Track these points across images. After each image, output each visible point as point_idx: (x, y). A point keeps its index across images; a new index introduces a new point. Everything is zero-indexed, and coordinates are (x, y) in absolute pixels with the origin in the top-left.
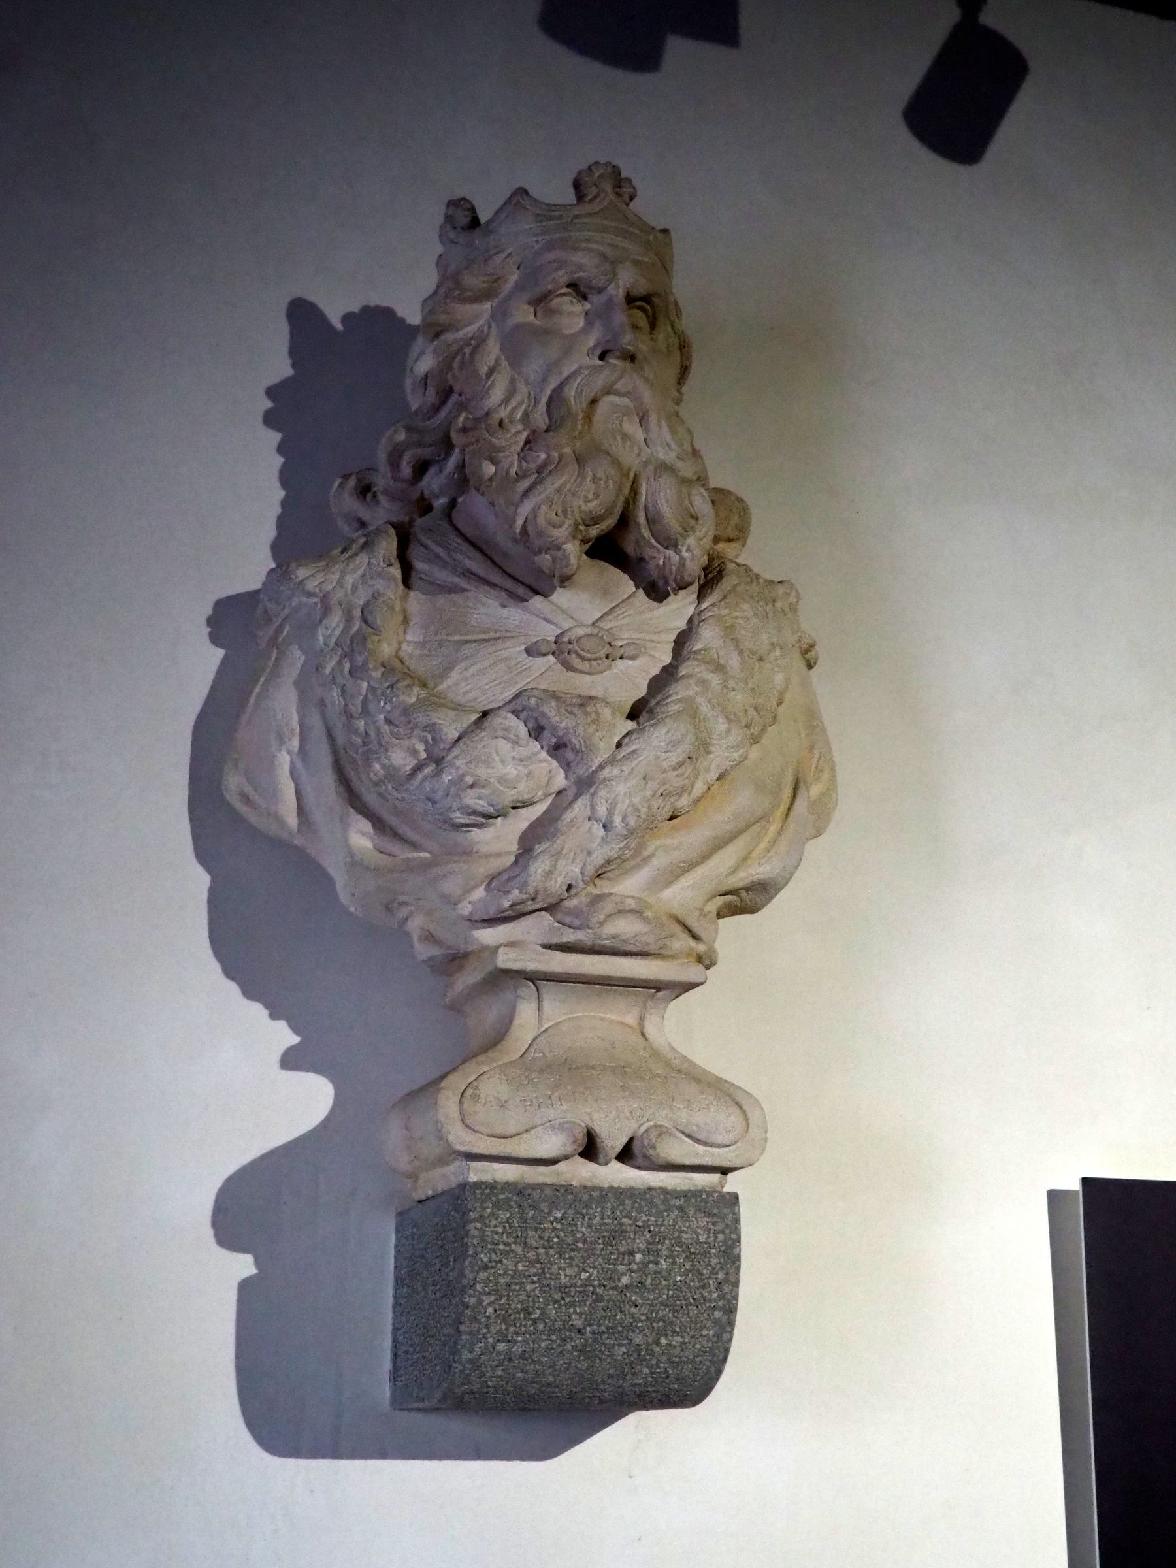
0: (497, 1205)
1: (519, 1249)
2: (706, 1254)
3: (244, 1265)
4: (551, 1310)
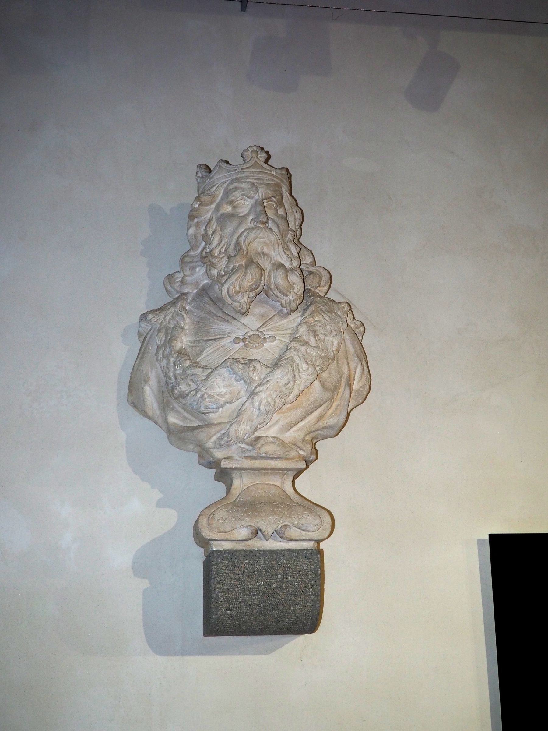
0: (223, 559)
1: (232, 575)
2: (307, 574)
3: (145, 584)
4: (246, 598)
